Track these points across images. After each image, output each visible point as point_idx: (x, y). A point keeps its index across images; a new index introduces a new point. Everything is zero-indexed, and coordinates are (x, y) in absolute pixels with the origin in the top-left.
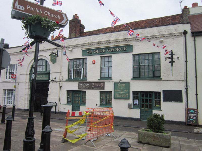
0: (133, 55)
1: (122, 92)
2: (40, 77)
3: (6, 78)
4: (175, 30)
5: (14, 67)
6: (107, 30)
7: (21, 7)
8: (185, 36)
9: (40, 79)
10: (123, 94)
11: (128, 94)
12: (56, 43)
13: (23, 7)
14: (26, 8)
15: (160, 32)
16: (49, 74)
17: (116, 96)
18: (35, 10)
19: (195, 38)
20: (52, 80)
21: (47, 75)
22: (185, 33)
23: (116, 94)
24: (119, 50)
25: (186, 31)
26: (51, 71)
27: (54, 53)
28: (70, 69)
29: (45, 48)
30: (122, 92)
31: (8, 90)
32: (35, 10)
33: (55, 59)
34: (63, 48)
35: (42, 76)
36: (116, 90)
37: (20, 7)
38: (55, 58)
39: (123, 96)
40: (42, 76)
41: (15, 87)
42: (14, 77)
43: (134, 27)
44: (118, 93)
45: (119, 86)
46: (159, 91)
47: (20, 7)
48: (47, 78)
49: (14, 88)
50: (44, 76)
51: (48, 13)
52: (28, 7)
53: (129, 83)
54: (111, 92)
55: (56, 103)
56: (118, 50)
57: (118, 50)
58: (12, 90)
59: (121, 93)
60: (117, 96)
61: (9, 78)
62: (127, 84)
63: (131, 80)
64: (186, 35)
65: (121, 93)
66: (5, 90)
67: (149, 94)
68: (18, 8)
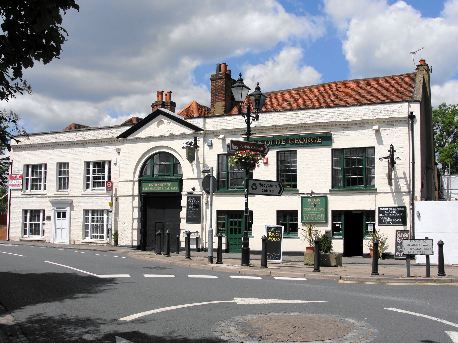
0: (334, 152)
1: (315, 211)
2: (161, 187)
3: (88, 187)
4: (398, 112)
5: (105, 167)
6: (285, 96)
7: (236, 147)
8: (413, 122)
9: (163, 189)
10: (316, 215)
11: (324, 216)
12: (189, 122)
13: (237, 147)
14: (239, 147)
15: (375, 113)
16: (180, 181)
17: (305, 219)
18: (245, 147)
19: (260, 260)
20: (189, 191)
21: (177, 184)
22: (412, 117)
23: (305, 215)
24: (309, 142)
25: (413, 114)
26: (183, 176)
27: (191, 144)
28: (220, 173)
29: (171, 132)
30: (315, 211)
31: (32, 211)
32: (245, 147)
33: (192, 155)
34: (207, 134)
35: (167, 185)
36: (304, 209)
37: (235, 148)
38: (193, 152)
39: (316, 219)
40: (167, 185)
41: (111, 204)
42: (109, 186)
43: (334, 94)
44: (309, 214)
45: (311, 202)
46: (374, 209)
47: (235, 148)
48: (177, 189)
49: (109, 208)
50: (169, 184)
51: (254, 148)
52: (240, 146)
53: (326, 197)
54: (297, 212)
55: (197, 232)
56: (306, 142)
57: (306, 142)
58: (102, 211)
59: (313, 213)
60: (306, 218)
61: (32, 189)
62: (325, 199)
63: (329, 192)
64: (413, 120)
65: (313, 213)
66: (25, 211)
67: (63, 213)
68: (234, 148)
